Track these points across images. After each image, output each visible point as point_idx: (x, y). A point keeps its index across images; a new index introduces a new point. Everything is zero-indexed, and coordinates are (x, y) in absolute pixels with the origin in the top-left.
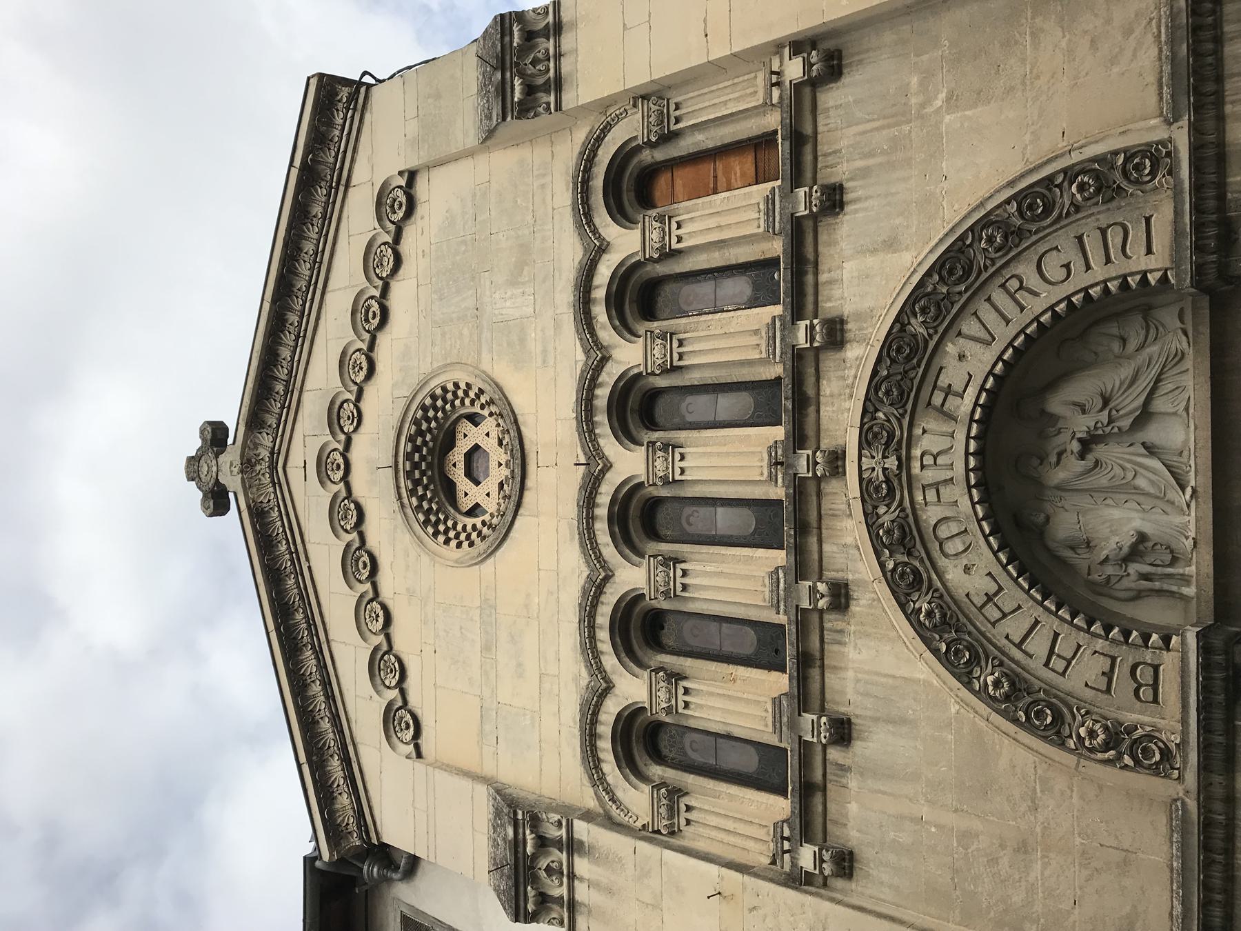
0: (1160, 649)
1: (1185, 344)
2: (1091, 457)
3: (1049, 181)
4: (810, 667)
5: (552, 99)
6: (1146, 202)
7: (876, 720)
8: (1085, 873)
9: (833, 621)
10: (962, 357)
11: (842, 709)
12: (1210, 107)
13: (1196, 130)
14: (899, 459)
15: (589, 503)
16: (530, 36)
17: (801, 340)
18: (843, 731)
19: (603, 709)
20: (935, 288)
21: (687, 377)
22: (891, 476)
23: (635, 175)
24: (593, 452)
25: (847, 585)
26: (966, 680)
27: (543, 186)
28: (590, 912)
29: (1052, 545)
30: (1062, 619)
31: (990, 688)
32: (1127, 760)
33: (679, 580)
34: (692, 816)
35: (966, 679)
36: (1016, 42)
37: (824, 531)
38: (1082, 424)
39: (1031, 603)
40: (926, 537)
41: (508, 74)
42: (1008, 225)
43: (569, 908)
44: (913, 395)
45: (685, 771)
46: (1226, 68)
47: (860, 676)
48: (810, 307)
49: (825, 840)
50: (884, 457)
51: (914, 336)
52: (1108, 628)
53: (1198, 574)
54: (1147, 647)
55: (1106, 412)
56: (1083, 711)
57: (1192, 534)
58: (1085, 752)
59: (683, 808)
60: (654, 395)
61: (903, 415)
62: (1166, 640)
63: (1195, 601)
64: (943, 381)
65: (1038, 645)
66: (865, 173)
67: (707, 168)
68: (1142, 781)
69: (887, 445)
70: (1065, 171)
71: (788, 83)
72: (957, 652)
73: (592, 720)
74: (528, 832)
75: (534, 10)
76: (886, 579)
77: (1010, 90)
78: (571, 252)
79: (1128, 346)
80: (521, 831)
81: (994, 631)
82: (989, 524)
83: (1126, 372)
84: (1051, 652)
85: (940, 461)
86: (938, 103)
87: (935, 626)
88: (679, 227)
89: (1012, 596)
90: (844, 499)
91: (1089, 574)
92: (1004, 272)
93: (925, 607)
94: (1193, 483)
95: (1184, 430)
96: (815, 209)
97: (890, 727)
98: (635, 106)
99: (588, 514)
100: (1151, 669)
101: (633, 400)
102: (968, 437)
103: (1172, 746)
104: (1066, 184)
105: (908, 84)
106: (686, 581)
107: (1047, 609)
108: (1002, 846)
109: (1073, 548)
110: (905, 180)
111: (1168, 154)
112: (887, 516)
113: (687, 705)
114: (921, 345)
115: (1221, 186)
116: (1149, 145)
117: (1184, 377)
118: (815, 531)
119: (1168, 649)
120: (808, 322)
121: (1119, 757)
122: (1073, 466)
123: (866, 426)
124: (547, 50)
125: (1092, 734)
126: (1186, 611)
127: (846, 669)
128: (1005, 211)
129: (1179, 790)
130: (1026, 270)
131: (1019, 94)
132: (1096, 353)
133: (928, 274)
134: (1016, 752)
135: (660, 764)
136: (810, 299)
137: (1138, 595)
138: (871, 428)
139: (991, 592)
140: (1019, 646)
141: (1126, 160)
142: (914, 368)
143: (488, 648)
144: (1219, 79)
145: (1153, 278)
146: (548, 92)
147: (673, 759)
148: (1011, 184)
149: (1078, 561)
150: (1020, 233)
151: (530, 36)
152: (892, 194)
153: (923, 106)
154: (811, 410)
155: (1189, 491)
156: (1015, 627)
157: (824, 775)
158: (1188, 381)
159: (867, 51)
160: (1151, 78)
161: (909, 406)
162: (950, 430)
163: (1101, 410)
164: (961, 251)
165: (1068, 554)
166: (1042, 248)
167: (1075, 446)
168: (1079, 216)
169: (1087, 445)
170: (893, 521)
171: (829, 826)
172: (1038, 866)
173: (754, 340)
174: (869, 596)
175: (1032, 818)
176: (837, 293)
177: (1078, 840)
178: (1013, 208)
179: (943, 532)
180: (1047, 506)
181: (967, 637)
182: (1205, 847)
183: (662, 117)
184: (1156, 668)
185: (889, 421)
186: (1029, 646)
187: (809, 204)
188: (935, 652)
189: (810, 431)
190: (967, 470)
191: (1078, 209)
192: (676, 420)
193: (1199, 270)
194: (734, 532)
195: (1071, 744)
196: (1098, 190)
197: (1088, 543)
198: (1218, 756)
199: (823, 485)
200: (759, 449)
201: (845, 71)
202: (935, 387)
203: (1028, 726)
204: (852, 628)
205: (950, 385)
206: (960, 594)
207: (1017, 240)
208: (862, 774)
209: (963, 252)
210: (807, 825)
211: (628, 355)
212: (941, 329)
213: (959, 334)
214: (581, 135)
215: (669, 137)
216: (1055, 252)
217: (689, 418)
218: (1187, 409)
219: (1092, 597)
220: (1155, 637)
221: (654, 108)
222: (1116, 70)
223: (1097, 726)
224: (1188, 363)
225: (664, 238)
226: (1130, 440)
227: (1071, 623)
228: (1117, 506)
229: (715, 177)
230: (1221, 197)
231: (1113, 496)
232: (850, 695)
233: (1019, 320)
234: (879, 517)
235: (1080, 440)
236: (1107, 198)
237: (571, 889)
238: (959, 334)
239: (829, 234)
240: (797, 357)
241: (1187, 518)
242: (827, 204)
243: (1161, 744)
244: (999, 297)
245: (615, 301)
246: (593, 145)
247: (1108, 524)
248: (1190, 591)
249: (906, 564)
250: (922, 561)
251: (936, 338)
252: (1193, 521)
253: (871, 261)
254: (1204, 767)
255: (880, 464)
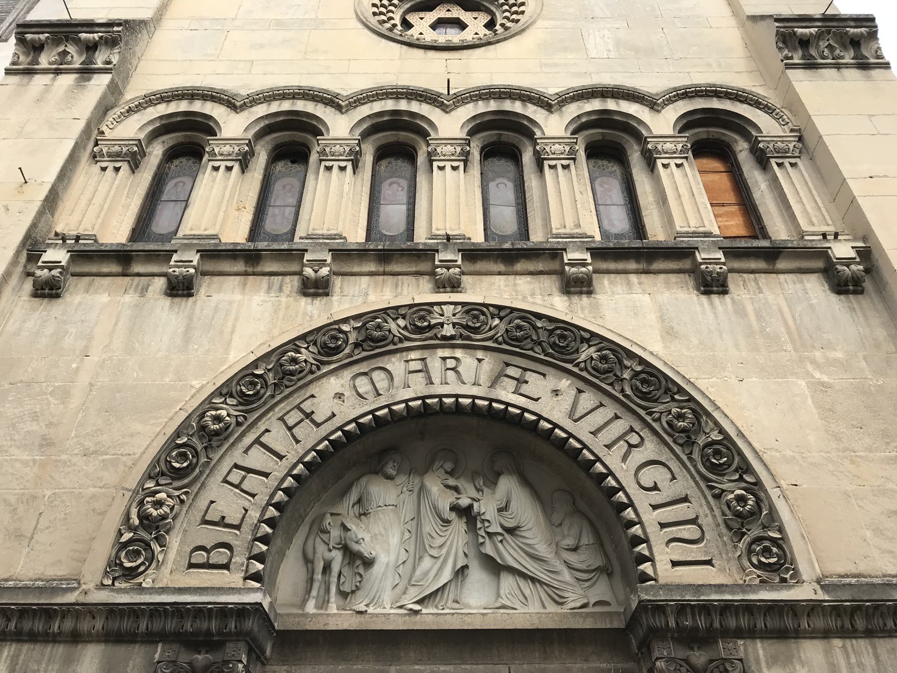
0: (247, 571)
1: (573, 605)
2: (453, 516)
3: (746, 468)
4: (246, 263)
5: (796, 61)
6: (729, 561)
7: (190, 318)
8: (13, 499)
9: (292, 283)
10: (556, 392)
11: (203, 291)
12: (839, 623)
13: (813, 607)
14: (452, 337)
15: (411, 94)
16: (855, 43)
17: (571, 255)
18: (180, 289)
19: (216, 105)
20: (627, 368)
21: (532, 176)
22: (435, 331)
23: (723, 138)
24: (462, 99)
25: (327, 295)
26: (224, 391)
27: (710, 65)
28: (23, 86)
29: (364, 480)
30: (283, 480)
31: (213, 413)
32: (127, 536)
33: (336, 164)
34: (110, 172)
35: (225, 391)
36: (888, 444)
37: (381, 278)
38: (487, 507)
39: (302, 452)
40: (374, 361)
41: (819, 24)
42: (697, 433)
43: (27, 69)
44: (517, 350)
45: (156, 174)
46: (881, 640)
47: (236, 305)
48: (604, 265)
49: (73, 275)
50: (454, 325)
51: (577, 351)
52: (271, 522)
53: (328, 615)
54: (249, 558)
55: (500, 530)
56: (184, 497)
57: (371, 610)
58: (139, 497)
59: (118, 165)
60: (514, 156)
61: (496, 341)
62: (256, 577)
63: (301, 612)
64: (529, 376)
65: (257, 459)
66: (741, 312)
67: (731, 197)
68: (103, 549)
69: (466, 327)
70: (758, 483)
71: (827, 245)
72: (254, 384)
73: (207, 96)
74: (100, 34)
75: (879, 48)
76: (331, 324)
77: (837, 437)
78: (652, 83)
79: (569, 553)
80: (103, 29)
81: (274, 419)
82: (386, 415)
83: (542, 549)
84: (249, 471)
85: (450, 373)
86: (817, 375)
87: (281, 365)
88: (678, 166)
89: (309, 435)
90: (415, 291)
91: (332, 514)
92: (646, 430)
93: (302, 357)
94: (424, 611)
95: (480, 604)
96: (703, 267)
97: (181, 330)
98: (792, 131)
99: (402, 93)
100: (225, 561)
101: (509, 136)
102: (474, 397)
103: (140, 579)
104: (744, 485)
105: (835, 350)
106: (335, 170)
107: (295, 466)
108: (50, 425)
109: (359, 501)
110: (737, 346)
111: (784, 580)
112: (395, 327)
113: (216, 169)
114: (568, 357)
115: (751, 634)
116: (793, 561)
117: (538, 604)
118: (381, 269)
119: (245, 579)
120: (589, 261)
121: (131, 528)
122: (445, 501)
123: (485, 309)
124: (842, 58)
125: (159, 504)
126: (292, 605)
127: (243, 293)
128: (712, 430)
129: (91, 586)
130: (650, 449)
131: (835, 446)
132: (560, 525)
133: (642, 361)
134: (145, 438)
135: (164, 154)
136: (612, 266)
137: (308, 561)
138: (483, 314)
139: (314, 417)
140: (257, 441)
141: (774, 541)
142: (544, 351)
143: (280, 24)
144: (869, 634)
145: (646, 567)
146: (803, 57)
147: (169, 168)
148: (740, 434)
149: (345, 504)
150: (689, 443)
151: (855, 43)
152: (721, 335)
153: (813, 362)
154: (501, 267)
155: (417, 607)
156: (277, 438)
157: (139, 275)
158: (534, 608)
159: (865, 316)
160: (862, 568)
161: (504, 346)
162: (481, 382)
163: (502, 526)
164: (667, 391)
165: (354, 496)
166: (674, 465)
167: (464, 502)
168: (710, 498)
169: (466, 513)
170: (390, 331)
171: (87, 279)
172: (25, 457)
173: (570, 223)
174: (316, 312)
175: (76, 451)
176: (619, 289)
177: (48, 493)
178: (715, 436)
179: (378, 376)
180: (401, 479)
181: (268, 394)
182: (25, 611)
183: (783, 154)
184: (226, 567)
185: (490, 329)
186: (256, 451)
187: (707, 261)
188: (255, 364)
189: (480, 266)
190: (440, 397)
191: (717, 497)
192: (490, 175)
193: (658, 608)
194: (382, 218)
195: (150, 484)
196: (738, 515)
197: (365, 514)
198: (122, 626)
199: (427, 277)
200: (462, 227)
201: (842, 297)
202: (525, 370)
203: (171, 444)
204: (284, 299)
205: (526, 382)
206: (313, 389)
207: (681, 441)
208: (136, 306)
209: (665, 393)
210: (90, 257)
211: (553, 126)
212: (584, 374)
213: (580, 391)
214: (760, 91)
215: (762, 159)
216: (669, 476)
217: (492, 185)
218: (504, 607)
219: (308, 520)
220: (260, 567)
221: (791, 146)
222: (869, 534)
223: (166, 509)
224: (552, 608)
225: (666, 153)
226: (472, 553)
227: (278, 488)
228: (402, 542)
229: (723, 205)
230: (739, 633)
231: (413, 538)
232: (216, 297)
233: (597, 444)
234: (395, 319)
235: (470, 507)
236: (731, 523)
237: (45, 71)
238: (580, 391)
239: (676, 283)
240: (555, 254)
241: (388, 607)
242: (709, 278)
243: (142, 569)
244: (619, 427)
245: (604, 119)
246: (751, 100)
247: (383, 531)
248: (311, 607)
249: (346, 342)
250: (349, 356)
251: (576, 370)
252: (384, 611)
253: (652, 318)
254: (112, 610)
255: (448, 320)
